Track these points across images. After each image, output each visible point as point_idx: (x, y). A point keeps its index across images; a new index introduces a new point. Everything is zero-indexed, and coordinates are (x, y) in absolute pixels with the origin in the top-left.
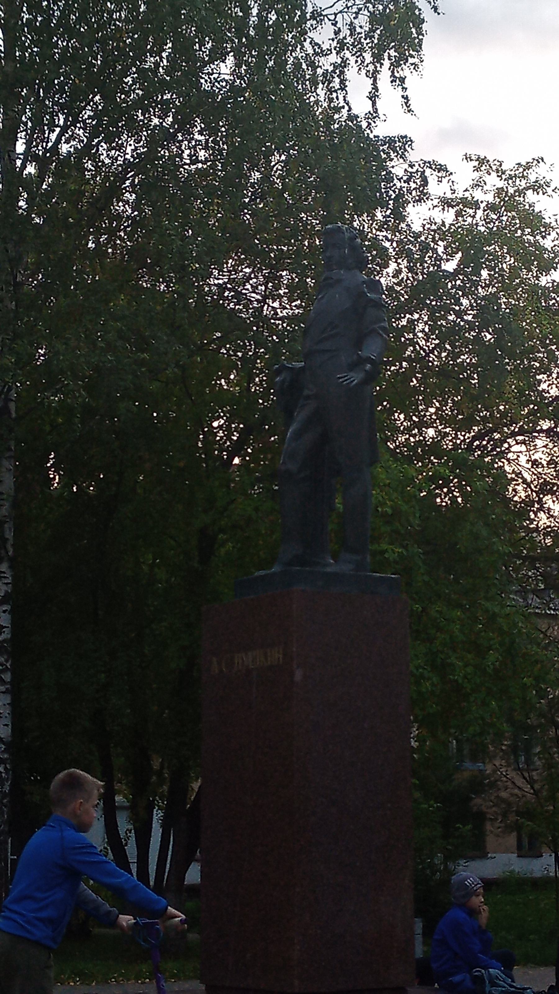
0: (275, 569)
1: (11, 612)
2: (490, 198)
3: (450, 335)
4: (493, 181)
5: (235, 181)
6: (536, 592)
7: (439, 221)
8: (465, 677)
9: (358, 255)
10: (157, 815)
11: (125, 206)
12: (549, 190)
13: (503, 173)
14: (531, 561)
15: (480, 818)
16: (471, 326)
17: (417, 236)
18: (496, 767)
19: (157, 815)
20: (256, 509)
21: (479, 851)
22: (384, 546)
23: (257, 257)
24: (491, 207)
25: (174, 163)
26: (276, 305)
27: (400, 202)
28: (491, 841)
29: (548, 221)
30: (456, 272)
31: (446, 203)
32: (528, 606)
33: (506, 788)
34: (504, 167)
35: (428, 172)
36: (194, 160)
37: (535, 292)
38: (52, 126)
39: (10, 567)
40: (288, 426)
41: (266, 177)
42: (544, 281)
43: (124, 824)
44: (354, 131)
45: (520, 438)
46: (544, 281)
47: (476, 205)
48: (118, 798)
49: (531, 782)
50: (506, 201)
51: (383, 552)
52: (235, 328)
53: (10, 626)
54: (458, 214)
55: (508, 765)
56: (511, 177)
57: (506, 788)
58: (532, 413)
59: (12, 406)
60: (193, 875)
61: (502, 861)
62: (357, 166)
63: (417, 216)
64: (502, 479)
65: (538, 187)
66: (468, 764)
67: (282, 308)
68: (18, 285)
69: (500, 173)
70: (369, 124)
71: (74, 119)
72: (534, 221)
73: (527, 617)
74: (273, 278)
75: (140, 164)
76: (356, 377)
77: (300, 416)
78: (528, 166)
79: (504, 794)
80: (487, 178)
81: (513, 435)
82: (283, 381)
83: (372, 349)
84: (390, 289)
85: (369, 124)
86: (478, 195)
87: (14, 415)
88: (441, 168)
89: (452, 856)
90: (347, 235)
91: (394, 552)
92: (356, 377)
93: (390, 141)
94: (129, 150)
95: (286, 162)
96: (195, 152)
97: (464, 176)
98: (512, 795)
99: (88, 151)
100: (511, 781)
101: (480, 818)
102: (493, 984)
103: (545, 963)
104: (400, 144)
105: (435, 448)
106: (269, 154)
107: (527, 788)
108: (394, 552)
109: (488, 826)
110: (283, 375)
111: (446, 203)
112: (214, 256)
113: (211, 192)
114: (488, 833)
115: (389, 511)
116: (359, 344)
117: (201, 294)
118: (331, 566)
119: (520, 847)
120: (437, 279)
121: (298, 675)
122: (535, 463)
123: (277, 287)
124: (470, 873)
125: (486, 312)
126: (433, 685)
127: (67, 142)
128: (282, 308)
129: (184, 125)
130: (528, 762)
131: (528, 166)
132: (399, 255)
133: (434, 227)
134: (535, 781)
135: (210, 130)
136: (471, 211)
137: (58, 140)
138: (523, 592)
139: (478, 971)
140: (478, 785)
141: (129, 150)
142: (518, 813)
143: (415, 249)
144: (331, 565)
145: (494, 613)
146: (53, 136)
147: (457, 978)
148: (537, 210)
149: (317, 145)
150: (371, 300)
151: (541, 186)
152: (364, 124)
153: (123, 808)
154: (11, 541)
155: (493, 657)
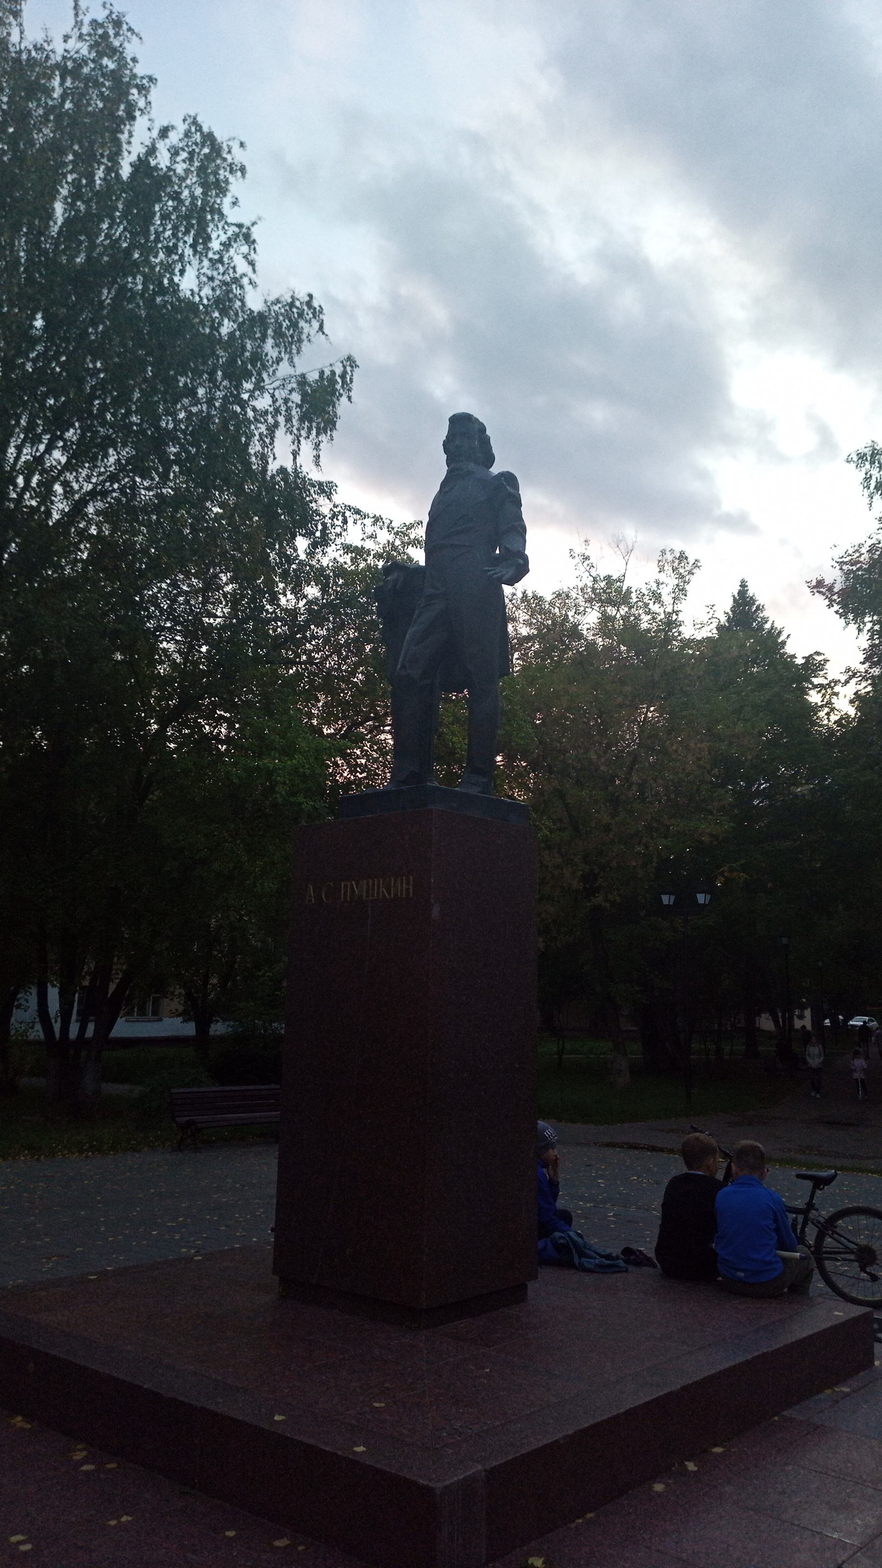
34: (393, 525)
51: (301, 804)
69: (390, 528)
80: (378, 531)
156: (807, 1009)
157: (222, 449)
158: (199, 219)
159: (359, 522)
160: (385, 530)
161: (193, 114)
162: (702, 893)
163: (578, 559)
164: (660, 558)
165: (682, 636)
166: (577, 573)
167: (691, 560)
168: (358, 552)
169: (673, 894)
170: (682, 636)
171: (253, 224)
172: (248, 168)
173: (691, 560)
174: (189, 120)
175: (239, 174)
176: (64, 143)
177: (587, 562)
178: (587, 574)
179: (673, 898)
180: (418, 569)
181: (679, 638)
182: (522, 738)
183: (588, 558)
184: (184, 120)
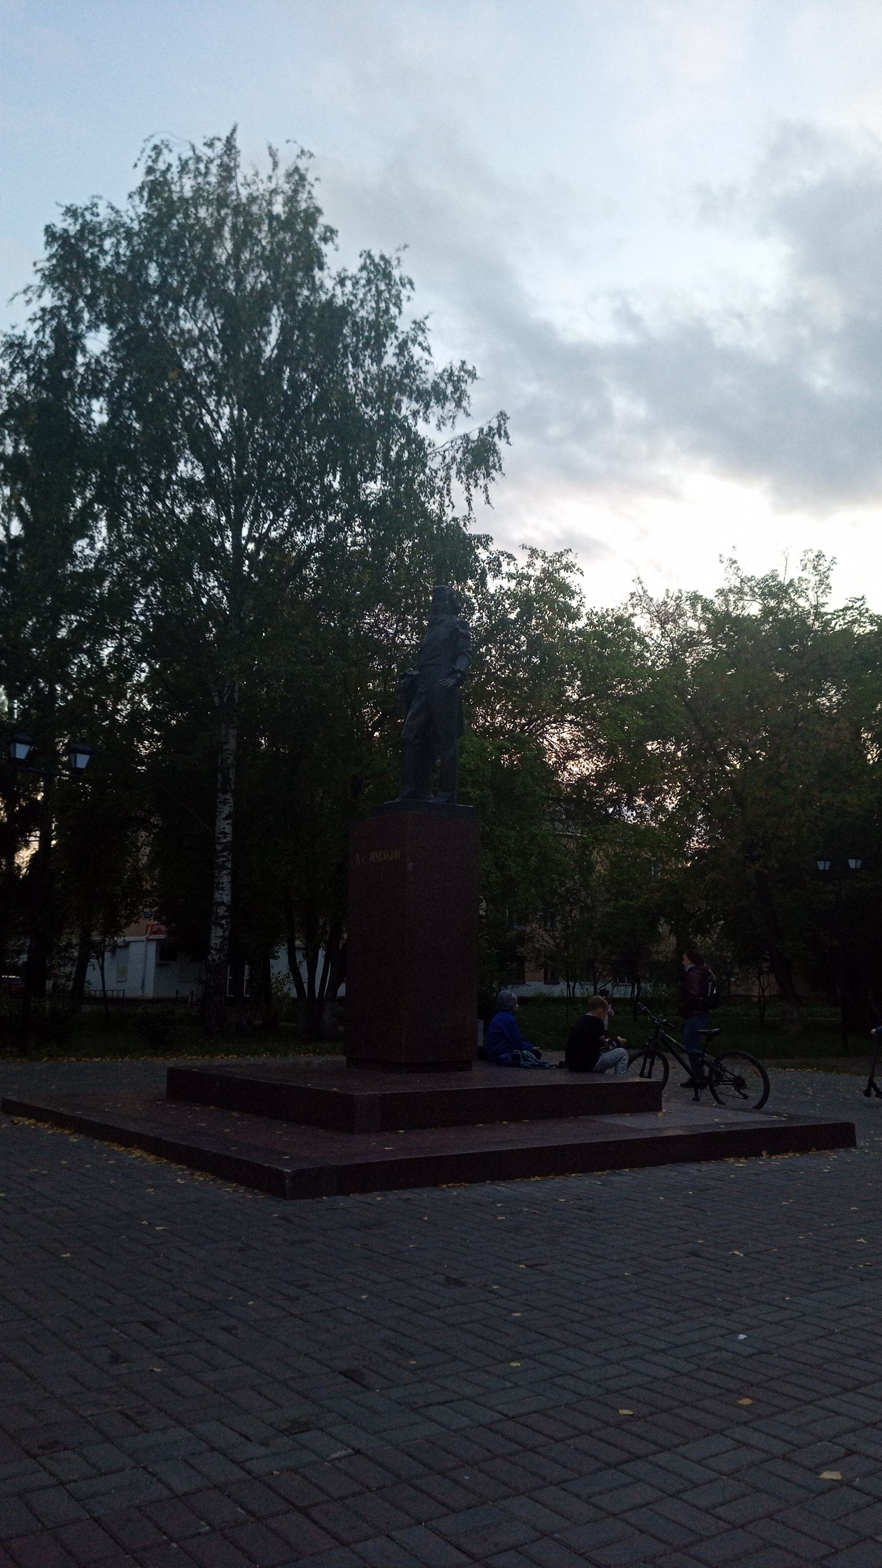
0: (397, 800)
1: (233, 824)
2: (538, 573)
3: (510, 658)
4: (539, 563)
5: (381, 556)
6: (560, 820)
7: (506, 588)
8: (516, 873)
9: (456, 605)
10: (322, 953)
11: (311, 571)
12: (575, 570)
13: (547, 558)
14: (557, 801)
15: (522, 960)
16: (524, 653)
17: (493, 596)
18: (533, 928)
19: (322, 953)
20: (389, 765)
21: (520, 979)
22: (469, 789)
23: (391, 605)
24: (539, 580)
25: (342, 543)
26: (403, 637)
27: (484, 575)
28: (527, 975)
29: (573, 589)
30: (516, 621)
31: (511, 576)
32: (555, 829)
33: (538, 941)
34: (547, 555)
35: (501, 559)
36: (354, 543)
37: (564, 633)
38: (265, 519)
39: (232, 796)
40: (408, 711)
41: (400, 557)
42: (571, 626)
43: (299, 957)
44: (455, 528)
45: (554, 725)
46: (571, 626)
47: (528, 578)
48: (297, 943)
49: (554, 938)
50: (548, 576)
51: (468, 793)
52: (379, 649)
53: (218, 805)
54: (519, 583)
55: (540, 928)
56: (550, 561)
57: (538, 941)
58: (562, 709)
59: (236, 696)
60: (342, 991)
61: (535, 987)
62: (455, 551)
63: (493, 585)
64: (542, 751)
65: (568, 567)
66: (516, 926)
67: (409, 639)
68: (242, 619)
69: (544, 557)
70: (465, 524)
71: (279, 514)
72: (565, 589)
73: (555, 836)
74: (402, 620)
75: (320, 545)
76: (451, 682)
77: (416, 704)
78: (561, 555)
79: (537, 946)
80: (535, 561)
81: (549, 723)
82: (405, 683)
83: (461, 664)
84: (475, 628)
85: (465, 524)
86: (531, 572)
87: (237, 701)
88: (510, 557)
89: (503, 983)
90: (448, 592)
91: (475, 793)
92: (451, 682)
93: (479, 538)
94: (313, 536)
95: (412, 547)
96: (356, 537)
97: (522, 559)
98: (542, 946)
99: (289, 534)
100: (542, 937)
101: (522, 960)
102: (525, 1060)
103: (559, 1049)
104: (485, 541)
105: (499, 731)
106: (401, 542)
107: (552, 942)
108: (475, 793)
109: (527, 965)
110: (406, 679)
111: (511, 576)
112: (366, 605)
113: (366, 565)
114: (526, 970)
115: (473, 768)
116: (454, 661)
117: (357, 631)
118: (432, 799)
119: (545, 979)
120: (504, 623)
121: (410, 866)
122: (562, 740)
123: (404, 626)
124: (513, 992)
125: (535, 644)
126: (496, 877)
127: (275, 530)
128: (409, 639)
129: (348, 519)
130: (553, 925)
131: (561, 555)
132: (482, 607)
133: (502, 591)
134: (557, 938)
135: (365, 524)
136: (526, 582)
137: (269, 528)
138: (552, 820)
139: (516, 1052)
140: (522, 939)
141: (313, 536)
142: (545, 957)
143: (491, 604)
144: (432, 799)
145: (535, 834)
146: (266, 526)
147: (504, 1056)
148: (567, 582)
149: (432, 536)
150: (462, 634)
151: (570, 567)
152: (462, 523)
153: (300, 949)
154: (233, 781)
155: (534, 862)
156: (340, 998)
157: (403, 511)
158: (379, 330)
159: (512, 564)
160: (540, 559)
161: (367, 249)
162: (853, 858)
163: (726, 564)
164: (803, 558)
165: (870, 613)
166: (726, 575)
167: (829, 558)
168: (522, 578)
169: (828, 860)
170: (870, 613)
171: (426, 318)
172: (414, 280)
173: (829, 558)
174: (365, 255)
175: (408, 286)
176: (192, 402)
177: (735, 565)
178: (735, 576)
179: (828, 864)
180: (19, 878)
181: (866, 615)
182: (672, 727)
183: (735, 562)
184: (361, 256)
